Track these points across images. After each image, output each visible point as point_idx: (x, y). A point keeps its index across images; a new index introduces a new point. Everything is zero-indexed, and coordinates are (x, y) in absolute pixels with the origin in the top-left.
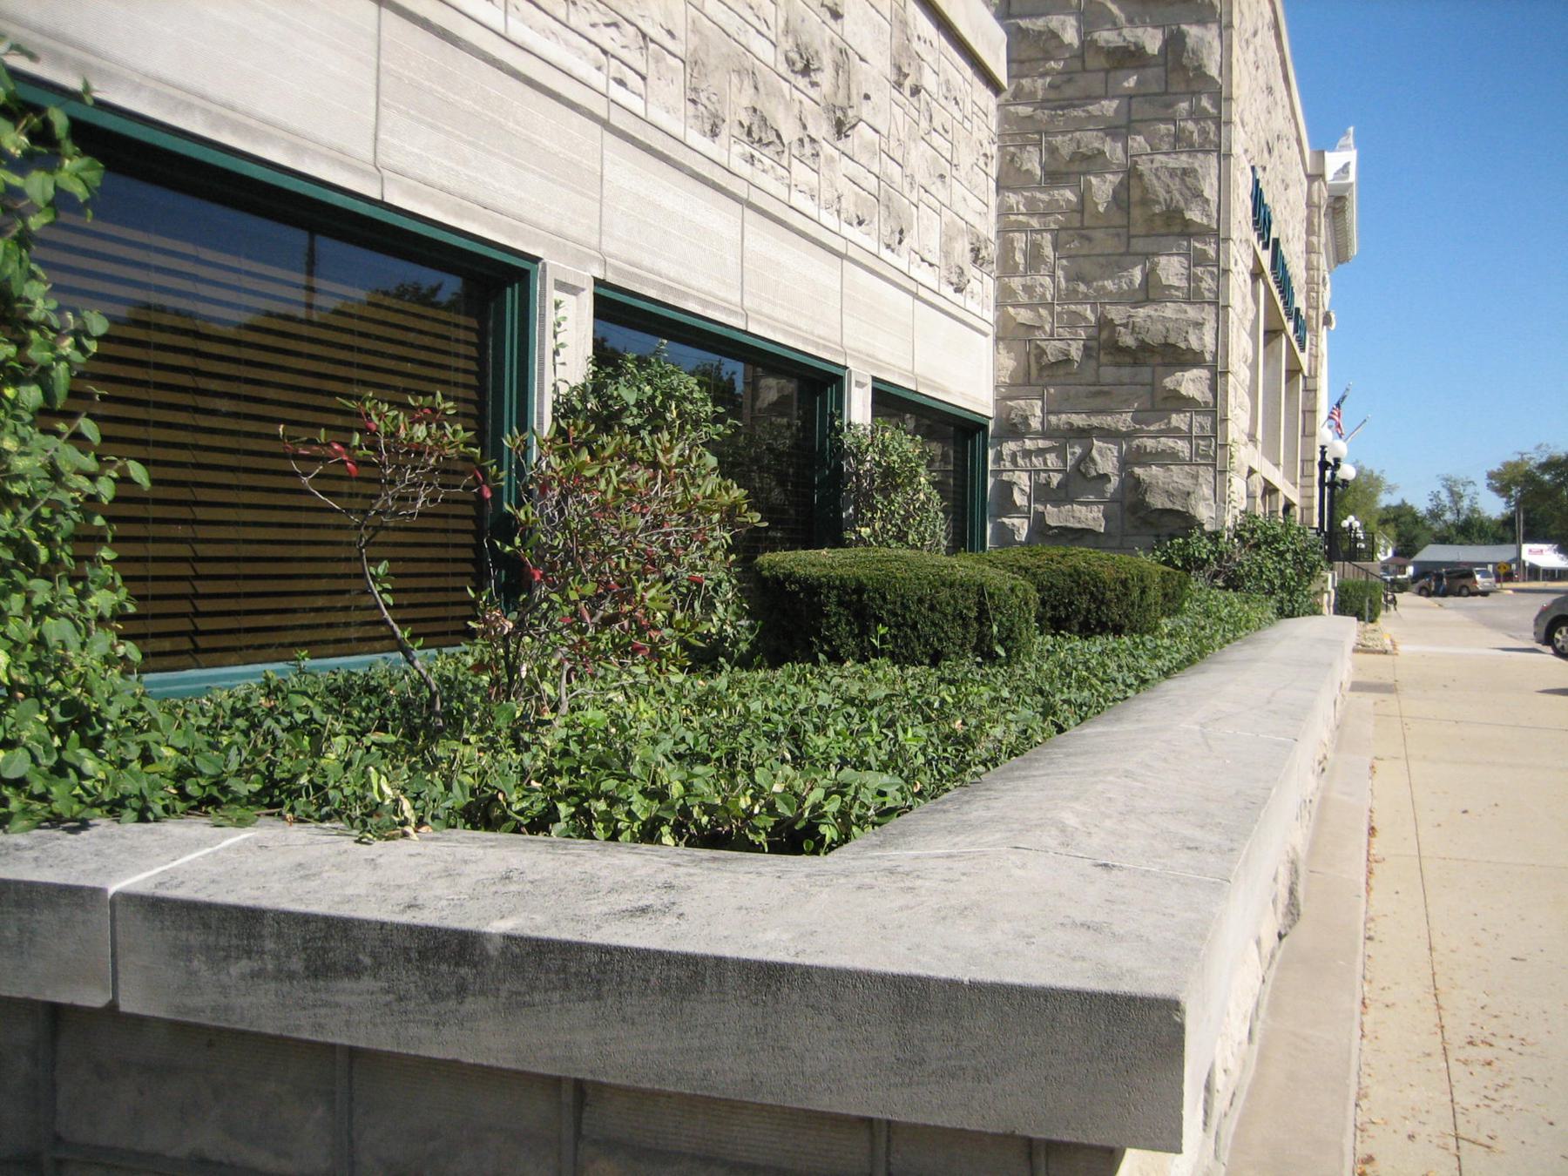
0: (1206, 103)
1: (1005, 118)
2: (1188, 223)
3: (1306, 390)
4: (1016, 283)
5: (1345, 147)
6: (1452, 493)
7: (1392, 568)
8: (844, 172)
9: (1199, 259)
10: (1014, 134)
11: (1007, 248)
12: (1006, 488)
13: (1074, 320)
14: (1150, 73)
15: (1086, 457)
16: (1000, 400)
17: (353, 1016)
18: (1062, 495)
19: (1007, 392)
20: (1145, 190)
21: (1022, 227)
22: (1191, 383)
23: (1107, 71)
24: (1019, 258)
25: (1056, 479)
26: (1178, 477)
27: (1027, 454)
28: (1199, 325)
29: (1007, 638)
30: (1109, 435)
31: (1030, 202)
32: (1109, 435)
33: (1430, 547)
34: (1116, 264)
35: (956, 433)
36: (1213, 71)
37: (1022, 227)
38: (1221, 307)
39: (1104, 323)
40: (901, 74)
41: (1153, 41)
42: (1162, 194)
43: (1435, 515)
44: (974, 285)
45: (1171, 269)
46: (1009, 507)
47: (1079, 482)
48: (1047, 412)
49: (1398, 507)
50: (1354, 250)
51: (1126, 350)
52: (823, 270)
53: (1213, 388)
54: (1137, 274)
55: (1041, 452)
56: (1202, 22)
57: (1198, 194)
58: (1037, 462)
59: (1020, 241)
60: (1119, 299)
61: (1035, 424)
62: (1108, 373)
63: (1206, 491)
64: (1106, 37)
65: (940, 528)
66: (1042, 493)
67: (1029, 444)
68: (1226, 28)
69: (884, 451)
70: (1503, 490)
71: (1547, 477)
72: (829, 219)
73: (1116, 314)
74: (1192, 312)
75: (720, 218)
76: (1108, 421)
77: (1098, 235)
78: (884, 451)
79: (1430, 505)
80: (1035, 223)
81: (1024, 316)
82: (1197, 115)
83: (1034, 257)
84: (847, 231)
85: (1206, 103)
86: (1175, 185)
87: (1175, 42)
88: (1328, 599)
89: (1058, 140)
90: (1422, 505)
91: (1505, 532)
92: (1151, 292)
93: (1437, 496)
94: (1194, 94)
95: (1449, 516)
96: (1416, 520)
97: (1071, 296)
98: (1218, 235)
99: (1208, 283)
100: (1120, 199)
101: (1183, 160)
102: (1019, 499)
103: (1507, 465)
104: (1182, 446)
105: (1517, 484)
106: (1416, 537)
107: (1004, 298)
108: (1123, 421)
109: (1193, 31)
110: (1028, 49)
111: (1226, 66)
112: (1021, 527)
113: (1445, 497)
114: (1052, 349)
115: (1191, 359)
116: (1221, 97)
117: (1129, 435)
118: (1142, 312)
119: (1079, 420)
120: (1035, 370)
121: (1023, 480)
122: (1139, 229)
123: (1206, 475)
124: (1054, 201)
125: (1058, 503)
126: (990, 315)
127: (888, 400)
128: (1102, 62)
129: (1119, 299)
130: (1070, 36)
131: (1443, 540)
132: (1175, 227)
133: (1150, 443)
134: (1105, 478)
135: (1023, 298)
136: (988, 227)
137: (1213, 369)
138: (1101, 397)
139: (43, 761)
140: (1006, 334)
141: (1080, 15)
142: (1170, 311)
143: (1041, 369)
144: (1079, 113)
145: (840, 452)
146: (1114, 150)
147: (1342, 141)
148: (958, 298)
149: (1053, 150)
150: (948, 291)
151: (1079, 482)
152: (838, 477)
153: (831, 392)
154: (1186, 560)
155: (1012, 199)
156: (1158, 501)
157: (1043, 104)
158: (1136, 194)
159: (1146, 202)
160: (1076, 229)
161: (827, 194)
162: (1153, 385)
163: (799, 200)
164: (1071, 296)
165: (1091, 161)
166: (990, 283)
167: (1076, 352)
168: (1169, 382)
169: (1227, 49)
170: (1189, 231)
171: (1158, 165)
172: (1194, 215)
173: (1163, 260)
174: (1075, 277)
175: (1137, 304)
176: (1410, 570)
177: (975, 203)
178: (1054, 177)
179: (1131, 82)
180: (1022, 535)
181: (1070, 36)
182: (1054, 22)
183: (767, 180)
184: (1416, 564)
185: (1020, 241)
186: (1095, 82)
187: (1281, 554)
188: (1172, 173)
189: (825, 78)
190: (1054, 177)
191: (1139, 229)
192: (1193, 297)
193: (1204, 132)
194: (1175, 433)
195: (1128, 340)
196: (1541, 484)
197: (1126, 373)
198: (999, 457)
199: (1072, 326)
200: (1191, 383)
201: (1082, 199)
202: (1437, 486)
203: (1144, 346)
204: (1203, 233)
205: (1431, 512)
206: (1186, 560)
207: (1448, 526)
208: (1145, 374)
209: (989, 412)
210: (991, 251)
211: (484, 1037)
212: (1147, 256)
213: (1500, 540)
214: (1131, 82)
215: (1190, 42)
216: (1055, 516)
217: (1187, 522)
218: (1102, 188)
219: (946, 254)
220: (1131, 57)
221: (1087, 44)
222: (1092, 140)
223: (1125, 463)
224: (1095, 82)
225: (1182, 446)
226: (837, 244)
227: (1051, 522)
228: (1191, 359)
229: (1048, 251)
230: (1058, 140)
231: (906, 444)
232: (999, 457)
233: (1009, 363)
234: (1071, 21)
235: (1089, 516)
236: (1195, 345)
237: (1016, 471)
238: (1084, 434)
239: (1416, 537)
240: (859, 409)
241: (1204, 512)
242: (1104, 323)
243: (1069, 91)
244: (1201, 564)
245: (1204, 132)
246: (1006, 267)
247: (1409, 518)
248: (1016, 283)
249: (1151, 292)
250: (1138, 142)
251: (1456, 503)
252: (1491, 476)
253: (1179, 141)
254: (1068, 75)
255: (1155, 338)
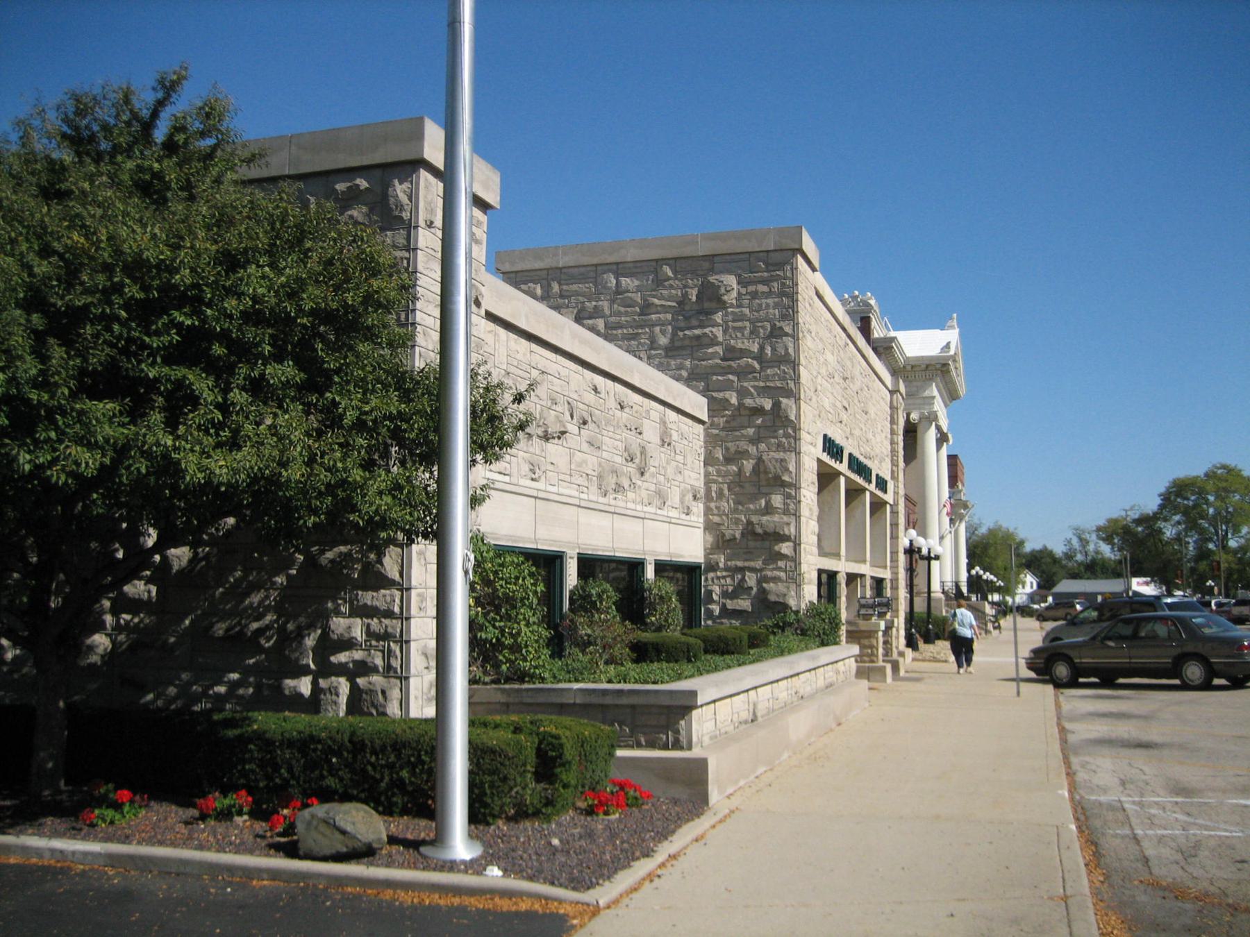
0: (790, 431)
1: (707, 435)
2: (783, 481)
3: (892, 512)
4: (713, 505)
5: (952, 327)
6: (1081, 539)
7: (1037, 598)
8: (646, 486)
9: (789, 496)
10: (711, 441)
11: (708, 490)
12: (709, 593)
13: (737, 521)
14: (767, 418)
15: (743, 579)
16: (706, 556)
17: (608, 700)
18: (733, 595)
19: (709, 552)
20: (766, 468)
21: (715, 482)
22: (786, 548)
23: (750, 416)
24: (714, 494)
25: (730, 588)
26: (781, 587)
27: (718, 578)
28: (788, 524)
29: (695, 656)
30: (752, 570)
31: (718, 471)
32: (752, 570)
33: (1064, 581)
34: (754, 498)
35: (691, 571)
36: (793, 418)
37: (715, 482)
38: (797, 516)
39: (749, 523)
40: (663, 442)
41: (768, 405)
42: (773, 470)
43: (1069, 556)
44: (695, 510)
45: (777, 500)
46: (712, 601)
47: (740, 590)
48: (726, 560)
49: (1041, 551)
50: (962, 391)
51: (758, 535)
52: (636, 526)
53: (795, 550)
54: (763, 502)
55: (724, 577)
56: (788, 397)
57: (787, 470)
58: (723, 581)
59: (714, 487)
60: (756, 512)
61: (721, 565)
62: (752, 544)
63: (793, 593)
64: (748, 402)
65: (679, 617)
66: (725, 594)
67: (719, 574)
68: (798, 399)
69: (660, 590)
70: (1108, 540)
71: (1140, 529)
72: (639, 508)
73: (754, 519)
74: (785, 519)
75: (604, 521)
76: (752, 564)
77: (747, 485)
78: (660, 590)
79: (1065, 549)
80: (720, 480)
81: (716, 519)
82: (787, 436)
83: (720, 494)
84: (645, 509)
85: (790, 431)
86: (778, 465)
87: (777, 405)
88: (843, 638)
89: (729, 445)
90: (1059, 549)
91: (1113, 571)
92: (769, 510)
93: (1069, 542)
94: (786, 427)
95: (1079, 557)
96: (1055, 561)
97: (736, 511)
98: (796, 486)
99: (792, 506)
100: (756, 470)
101: (781, 455)
102: (715, 597)
103: (1110, 521)
104: (782, 574)
105: (1117, 535)
106: (1054, 574)
107: (708, 511)
108: (758, 564)
109: (784, 401)
110: (716, 407)
111: (798, 416)
112: (716, 609)
113: (1075, 542)
114: (728, 534)
115: (786, 538)
116: (797, 429)
117: (761, 570)
118: (765, 518)
119: (740, 564)
120: (720, 542)
121: (717, 589)
122: (764, 483)
123: (793, 586)
124: (728, 471)
125: (731, 599)
126: (701, 520)
127: (661, 567)
128: (747, 412)
129: (756, 512)
130: (734, 401)
131: (1075, 576)
132: (778, 483)
133: (769, 574)
134: (751, 588)
135: (715, 511)
136: (700, 484)
137: (795, 542)
138: (749, 554)
139: (882, 625)
140: (709, 527)
141: (738, 392)
142: (776, 518)
143: (724, 542)
144: (737, 433)
145: (643, 590)
146: (752, 449)
147: (950, 323)
148: (688, 518)
149: (727, 449)
150: (683, 516)
151: (740, 590)
152: (643, 599)
153: (640, 568)
154: (784, 623)
155: (710, 469)
156: (772, 598)
157: (723, 429)
158: (762, 469)
159: (766, 472)
160: (738, 482)
161: (639, 499)
162: (770, 549)
163: (630, 505)
164: (736, 511)
165: (744, 454)
166: (701, 506)
167: (738, 536)
168: (776, 548)
169: (799, 408)
170: (784, 484)
171: (771, 456)
172: (786, 478)
173: (773, 497)
174: (737, 503)
175: (763, 515)
176: (1050, 599)
177: (695, 475)
178: (728, 460)
179: (759, 421)
180: (717, 612)
181: (734, 401)
182: (727, 394)
183: (620, 502)
184: (1055, 596)
185: (714, 487)
186: (745, 420)
187: (823, 620)
188: (776, 460)
189: (637, 461)
190: (728, 460)
191: (764, 483)
192: (786, 512)
193: (789, 443)
194: (779, 569)
195: (759, 530)
196: (1135, 534)
197: (758, 544)
198: (706, 579)
199: (736, 523)
200: (786, 548)
201: (740, 470)
202: (1069, 535)
203: (766, 533)
204: (790, 485)
205: (1066, 554)
206: (784, 623)
207: (1080, 564)
208: (767, 544)
209: (702, 560)
210: (702, 492)
211: (624, 701)
212: (767, 494)
213: (1118, 575)
214: (759, 421)
215: (783, 406)
216: (730, 604)
217: (785, 607)
218: (748, 465)
219: (682, 502)
220: (759, 411)
221: (741, 405)
222: (744, 445)
223: (759, 582)
224: (745, 420)
225: (782, 574)
226: (642, 515)
227: (729, 607)
228: (786, 538)
229: (726, 492)
230: (729, 445)
231: (669, 588)
232: (706, 579)
233: (710, 539)
234: (734, 394)
235: (744, 604)
236: (787, 532)
237: (714, 585)
238: (742, 570)
239: (1054, 574)
240: (650, 573)
241: (792, 603)
242: (749, 523)
243: (734, 424)
244: (790, 624)
245: (789, 443)
246: (708, 497)
247: (1049, 560)
248: (713, 505)
249: (769, 510)
250: (763, 446)
251: (1084, 547)
252: (1099, 529)
253: (780, 446)
254: (733, 417)
255: (770, 529)
